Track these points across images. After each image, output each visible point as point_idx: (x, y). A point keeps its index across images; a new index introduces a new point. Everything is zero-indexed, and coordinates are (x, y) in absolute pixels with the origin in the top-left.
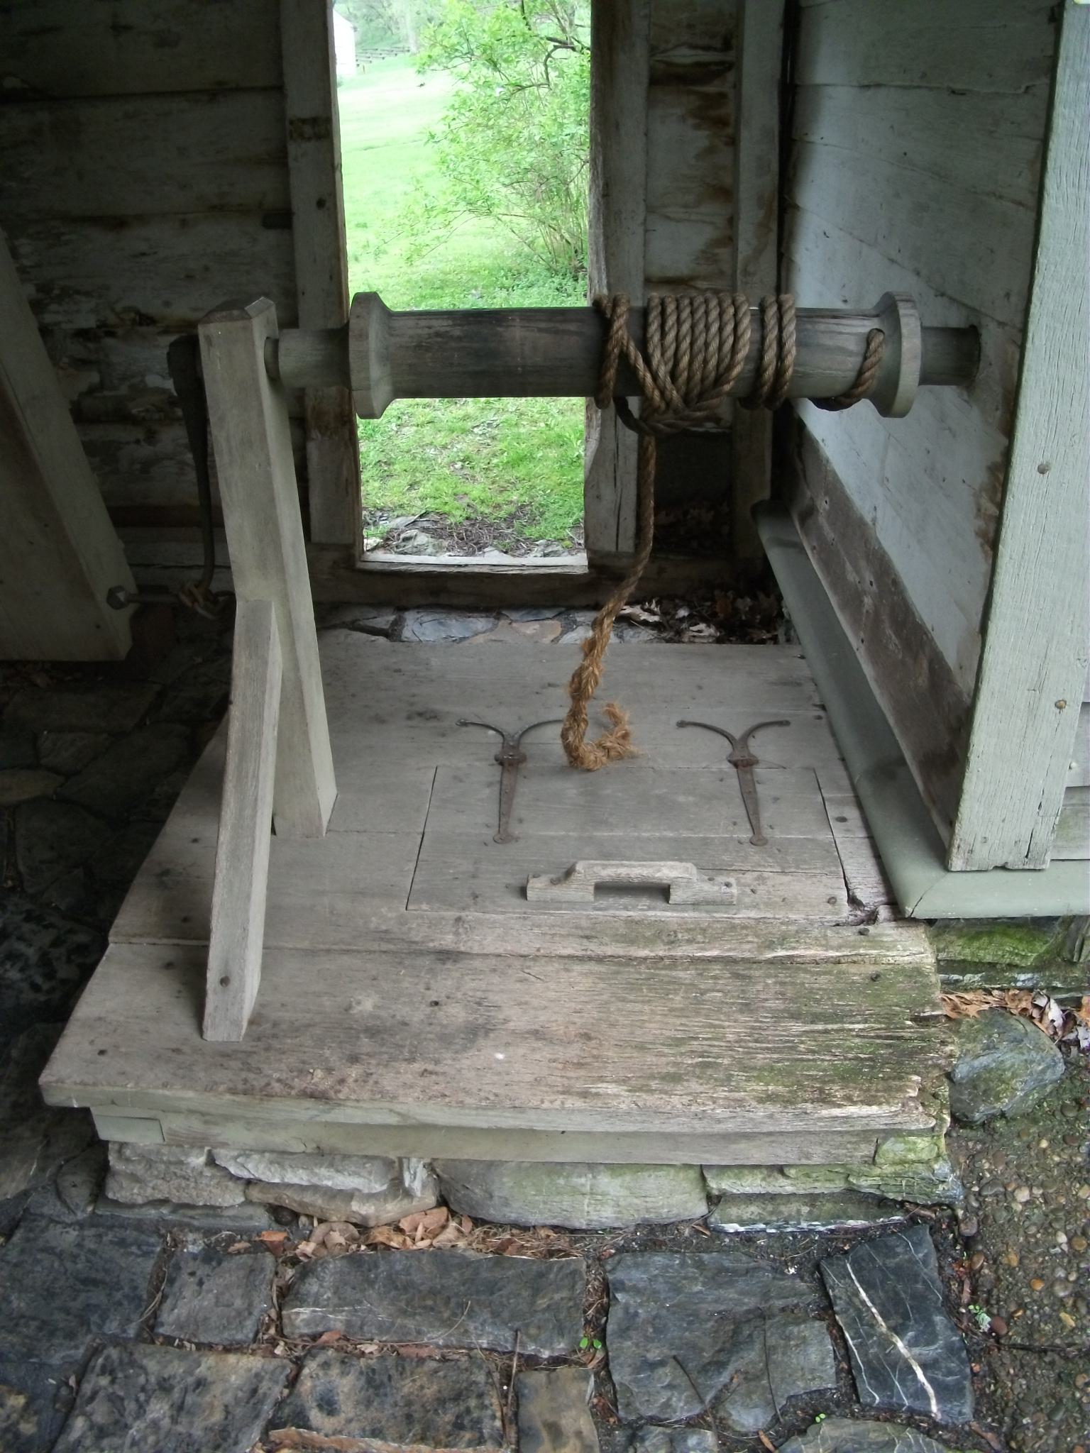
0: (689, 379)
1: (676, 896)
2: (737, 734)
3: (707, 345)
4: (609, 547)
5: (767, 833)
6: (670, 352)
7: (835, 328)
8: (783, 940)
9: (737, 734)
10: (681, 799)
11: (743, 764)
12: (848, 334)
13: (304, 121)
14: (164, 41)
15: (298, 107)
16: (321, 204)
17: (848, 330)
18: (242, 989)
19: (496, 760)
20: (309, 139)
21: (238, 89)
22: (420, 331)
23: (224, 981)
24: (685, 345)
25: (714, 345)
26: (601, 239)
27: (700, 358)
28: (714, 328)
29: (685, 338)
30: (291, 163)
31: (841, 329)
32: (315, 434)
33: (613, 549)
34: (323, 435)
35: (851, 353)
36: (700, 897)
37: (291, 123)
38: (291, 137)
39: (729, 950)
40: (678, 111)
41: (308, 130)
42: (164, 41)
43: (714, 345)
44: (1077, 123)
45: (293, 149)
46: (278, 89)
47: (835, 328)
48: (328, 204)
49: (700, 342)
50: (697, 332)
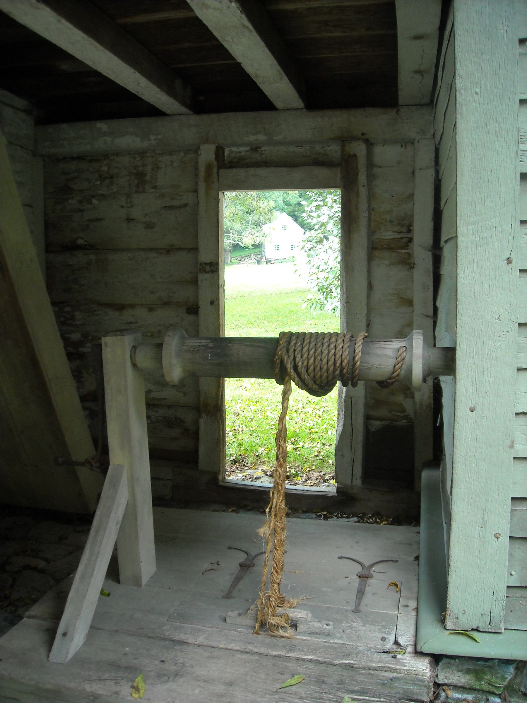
0: (314, 369)
1: (301, 628)
2: (367, 564)
3: (322, 352)
4: (349, 482)
5: (362, 608)
6: (305, 356)
7: (383, 346)
8: (348, 655)
9: (367, 564)
10: (324, 589)
11: (364, 577)
12: (389, 348)
13: (206, 264)
14: (149, 226)
15: (204, 257)
16: (212, 303)
17: (390, 347)
18: (71, 640)
19: (239, 565)
20: (208, 272)
21: (179, 249)
22: (196, 344)
23: (65, 635)
24: (311, 353)
25: (325, 352)
26: (345, 324)
27: (319, 358)
28: (326, 345)
29: (312, 349)
30: (199, 283)
31: (386, 346)
32: (204, 415)
33: (350, 483)
34: (207, 416)
35: (390, 357)
36: (313, 630)
37: (200, 264)
38: (200, 271)
39: (319, 657)
40: (387, 262)
41: (208, 268)
42: (149, 226)
43: (325, 352)
44: (469, 244)
45: (201, 277)
46: (195, 249)
47: (383, 346)
48: (215, 303)
49: (319, 351)
50: (317, 347)
